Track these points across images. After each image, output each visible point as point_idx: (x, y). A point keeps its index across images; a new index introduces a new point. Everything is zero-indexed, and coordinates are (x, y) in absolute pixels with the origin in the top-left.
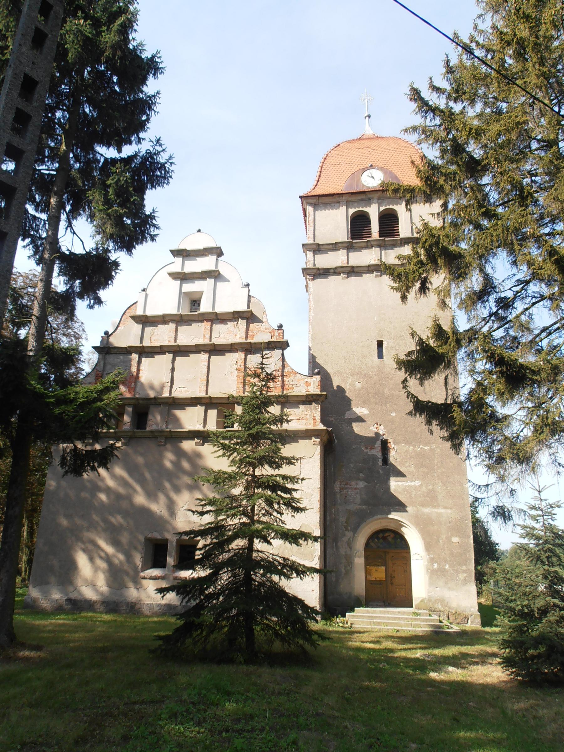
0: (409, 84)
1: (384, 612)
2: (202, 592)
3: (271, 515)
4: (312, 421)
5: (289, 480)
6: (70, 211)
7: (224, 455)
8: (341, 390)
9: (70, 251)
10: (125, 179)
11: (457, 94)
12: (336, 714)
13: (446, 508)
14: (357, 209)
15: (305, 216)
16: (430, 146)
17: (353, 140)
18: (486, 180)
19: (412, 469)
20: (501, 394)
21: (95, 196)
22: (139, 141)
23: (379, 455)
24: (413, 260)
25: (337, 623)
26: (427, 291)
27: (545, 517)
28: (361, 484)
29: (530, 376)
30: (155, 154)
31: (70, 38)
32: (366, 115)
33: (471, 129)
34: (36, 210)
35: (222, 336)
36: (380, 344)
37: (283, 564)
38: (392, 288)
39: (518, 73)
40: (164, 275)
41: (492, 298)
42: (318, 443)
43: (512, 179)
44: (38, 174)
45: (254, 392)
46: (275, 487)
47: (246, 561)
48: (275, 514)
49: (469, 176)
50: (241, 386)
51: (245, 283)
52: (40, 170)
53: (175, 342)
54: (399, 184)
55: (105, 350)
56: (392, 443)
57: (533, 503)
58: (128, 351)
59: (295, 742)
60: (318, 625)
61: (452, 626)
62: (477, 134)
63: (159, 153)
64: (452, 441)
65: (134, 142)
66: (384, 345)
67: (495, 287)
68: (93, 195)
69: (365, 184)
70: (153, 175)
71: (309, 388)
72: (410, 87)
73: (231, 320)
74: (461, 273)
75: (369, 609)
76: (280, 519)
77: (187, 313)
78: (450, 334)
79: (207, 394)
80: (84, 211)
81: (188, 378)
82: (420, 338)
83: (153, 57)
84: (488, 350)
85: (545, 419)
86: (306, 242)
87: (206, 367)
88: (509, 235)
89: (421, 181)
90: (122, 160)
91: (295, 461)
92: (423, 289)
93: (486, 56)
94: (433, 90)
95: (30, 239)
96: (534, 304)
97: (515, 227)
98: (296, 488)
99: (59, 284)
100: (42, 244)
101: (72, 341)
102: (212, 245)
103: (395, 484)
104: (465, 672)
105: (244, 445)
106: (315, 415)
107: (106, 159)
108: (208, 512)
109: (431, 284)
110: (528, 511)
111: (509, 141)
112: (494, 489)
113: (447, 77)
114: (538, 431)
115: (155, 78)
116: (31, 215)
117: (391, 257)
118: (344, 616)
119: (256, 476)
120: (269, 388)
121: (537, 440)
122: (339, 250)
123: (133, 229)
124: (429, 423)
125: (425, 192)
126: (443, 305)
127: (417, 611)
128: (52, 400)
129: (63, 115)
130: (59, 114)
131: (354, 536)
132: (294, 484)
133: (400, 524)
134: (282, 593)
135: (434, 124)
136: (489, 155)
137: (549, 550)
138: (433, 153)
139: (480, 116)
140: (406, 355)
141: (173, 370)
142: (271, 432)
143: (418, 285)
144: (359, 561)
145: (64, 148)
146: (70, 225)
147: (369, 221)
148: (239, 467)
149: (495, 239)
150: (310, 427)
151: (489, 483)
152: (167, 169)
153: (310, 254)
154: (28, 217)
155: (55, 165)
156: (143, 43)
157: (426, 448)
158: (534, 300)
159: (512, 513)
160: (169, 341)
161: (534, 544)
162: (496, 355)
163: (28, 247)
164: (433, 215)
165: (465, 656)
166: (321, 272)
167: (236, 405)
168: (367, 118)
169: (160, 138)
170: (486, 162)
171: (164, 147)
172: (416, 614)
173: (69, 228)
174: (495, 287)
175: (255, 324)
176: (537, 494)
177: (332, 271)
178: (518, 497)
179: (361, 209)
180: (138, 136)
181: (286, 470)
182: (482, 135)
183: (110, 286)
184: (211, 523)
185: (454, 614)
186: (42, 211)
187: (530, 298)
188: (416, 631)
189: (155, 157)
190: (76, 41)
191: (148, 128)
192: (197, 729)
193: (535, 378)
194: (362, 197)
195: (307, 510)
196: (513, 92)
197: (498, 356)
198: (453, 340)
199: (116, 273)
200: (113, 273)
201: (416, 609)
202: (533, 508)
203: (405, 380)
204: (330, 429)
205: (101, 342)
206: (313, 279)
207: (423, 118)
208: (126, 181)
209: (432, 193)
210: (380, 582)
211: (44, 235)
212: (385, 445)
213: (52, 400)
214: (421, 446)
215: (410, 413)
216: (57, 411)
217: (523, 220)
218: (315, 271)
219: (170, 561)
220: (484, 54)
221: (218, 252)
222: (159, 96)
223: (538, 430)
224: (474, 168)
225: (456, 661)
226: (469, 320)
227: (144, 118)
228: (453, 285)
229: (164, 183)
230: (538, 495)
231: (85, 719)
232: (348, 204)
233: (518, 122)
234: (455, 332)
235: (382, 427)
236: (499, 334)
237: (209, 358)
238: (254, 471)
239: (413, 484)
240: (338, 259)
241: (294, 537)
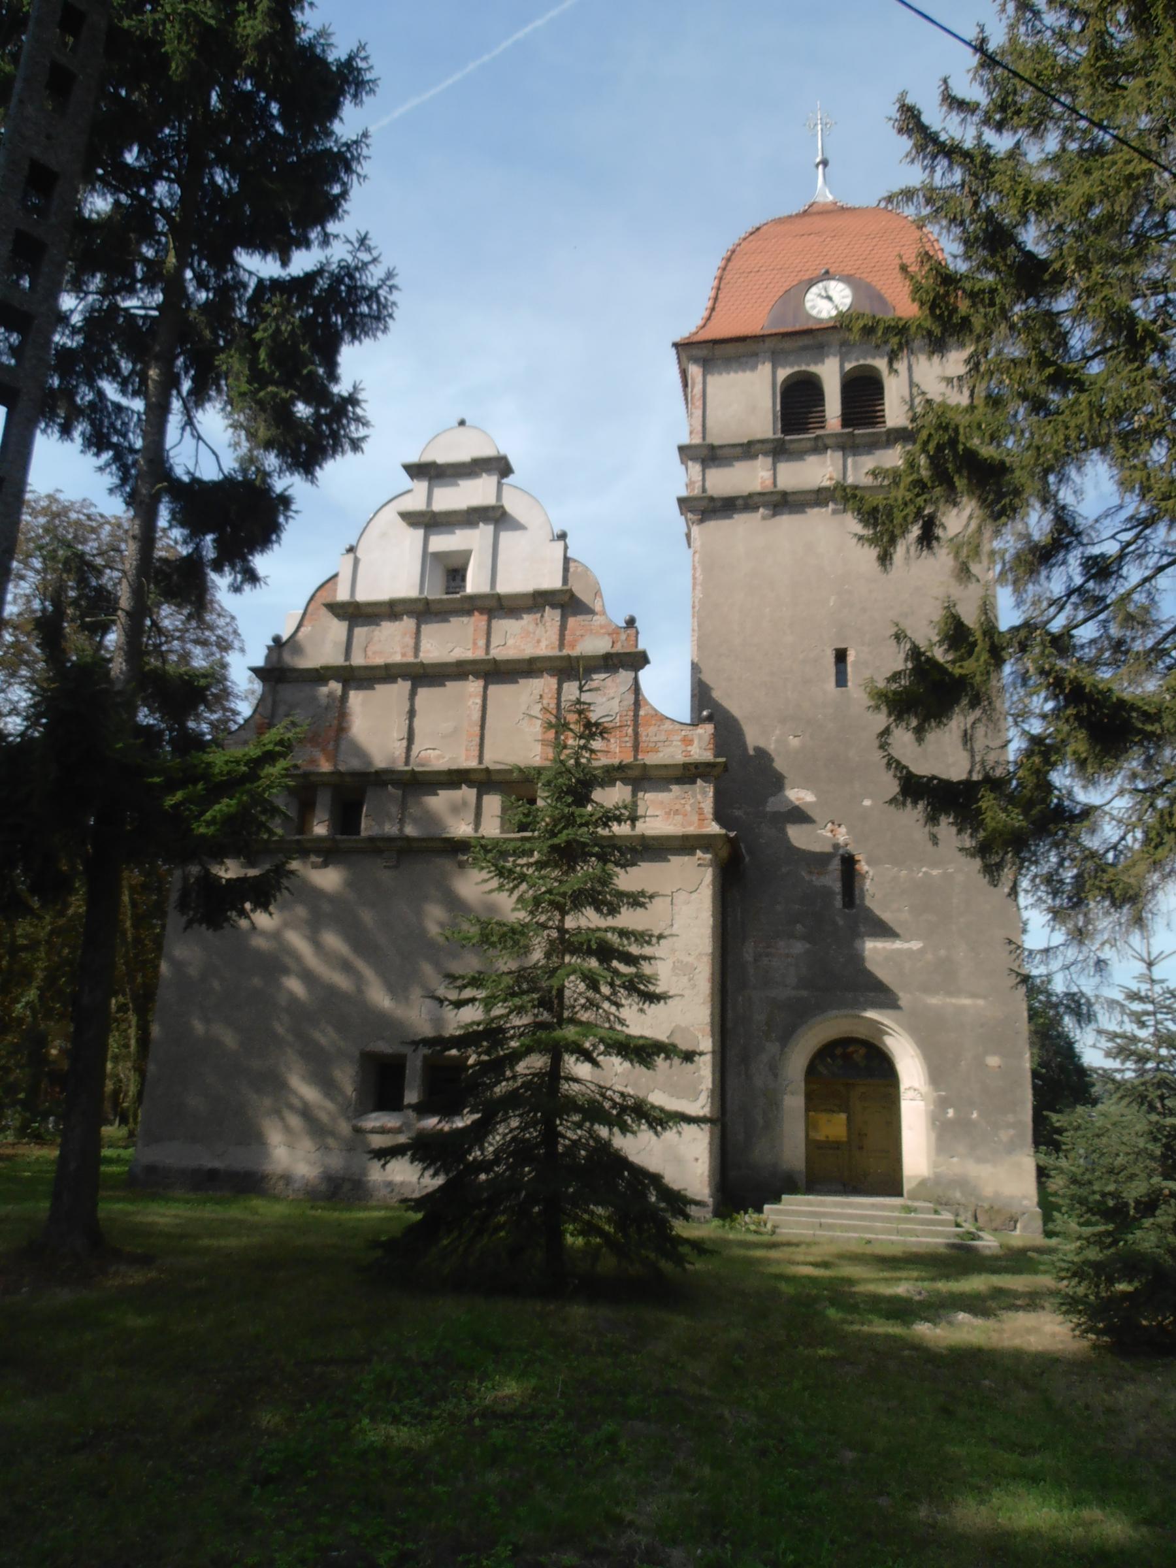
0: (895, 97)
1: (842, 1205)
2: (462, 1157)
3: (598, 1007)
4: (695, 818)
5: (633, 939)
6: (190, 393)
7: (501, 888)
9: (192, 474)
10: (289, 328)
11: (1003, 113)
12: (706, 1392)
13: (974, 996)
14: (796, 369)
15: (685, 385)
16: (944, 231)
17: (790, 217)
18: (1064, 303)
19: (905, 915)
20: (1082, 764)
21: (232, 362)
22: (326, 240)
23: (837, 887)
24: (903, 478)
25: (746, 1223)
26: (935, 543)
27: (1159, 1016)
28: (799, 947)
29: (1140, 726)
30: (357, 268)
31: (171, 30)
32: (818, 160)
33: (1027, 192)
34: (124, 392)
35: (510, 642)
36: (841, 656)
37: (621, 1105)
38: (861, 538)
39: (1136, 61)
40: (390, 515)
41: (1074, 560)
43: (1110, 303)
44: (124, 317)
45: (562, 762)
46: (605, 953)
47: (548, 1097)
48: (606, 1005)
49: (1024, 294)
51: (557, 531)
52: (126, 310)
53: (416, 655)
54: (874, 317)
55: (277, 672)
56: (863, 863)
57: (1134, 986)
58: (321, 675)
59: (612, 1440)
60: (701, 1227)
61: (980, 1233)
62: (1043, 200)
63: (365, 265)
64: (983, 858)
65: (316, 243)
66: (851, 657)
67: (1079, 534)
68: (228, 363)
69: (814, 313)
70: (355, 313)
71: (689, 748)
72: (898, 105)
73: (529, 609)
74: (1004, 507)
75: (811, 1197)
76: (615, 1016)
77: (438, 597)
78: (978, 635)
80: (219, 390)
81: (447, 732)
82: (913, 643)
83: (351, 59)
84: (1051, 669)
85: (1166, 817)
86: (686, 440)
87: (478, 707)
88: (1104, 424)
89: (920, 308)
90: (295, 280)
91: (647, 900)
92: (928, 538)
93: (1070, 26)
94: (950, 107)
95: (111, 453)
96: (1161, 569)
97: (1117, 407)
98: (648, 954)
99: (173, 540)
100: (135, 463)
101: (213, 654)
102: (487, 452)
103: (873, 948)
104: (990, 1323)
105: (542, 868)
106: (702, 805)
107: (261, 281)
108: (472, 1000)
109: (945, 528)
110: (1126, 1003)
111: (1110, 218)
112: (1061, 958)
113: (982, 77)
114: (1153, 841)
115: (356, 104)
116: (113, 403)
117: (860, 470)
118: (759, 1210)
119: (567, 931)
120: (592, 751)
121: (1150, 860)
123: (313, 428)
124: (932, 819)
125: (930, 333)
126: (964, 573)
127: (909, 1203)
128: (157, 780)
129: (169, 191)
130: (161, 188)
131: (782, 1050)
132: (642, 947)
133: (879, 1030)
134: (620, 1162)
135: (949, 184)
136: (1065, 251)
137: (1165, 1082)
138: (949, 248)
139: (1054, 161)
140: (888, 680)
141: (412, 713)
142: (597, 840)
143: (916, 531)
144: (794, 1102)
145: (174, 260)
146: (190, 422)
148: (531, 912)
149: (1073, 435)
150: (692, 830)
151: (1053, 944)
152: (382, 299)
153: (695, 468)
154: (106, 407)
155: (156, 296)
156: (330, 31)
157: (935, 872)
158: (1165, 560)
159: (1097, 1007)
160: (404, 655)
161: (1134, 1071)
162: (1067, 682)
163: (108, 470)
164: (949, 381)
165: (998, 1293)
166: (719, 504)
168: (821, 167)
169: (367, 234)
170: (1057, 266)
171: (375, 253)
172: (908, 1209)
173: (188, 429)
174: (1079, 534)
175: (580, 618)
176: (1141, 967)
177: (740, 502)
178: (1110, 975)
179: (804, 368)
180: (323, 228)
181: (628, 918)
182: (1053, 204)
183: (276, 546)
184: (478, 1024)
185: (986, 1211)
186: (135, 394)
187: (1157, 556)
188: (905, 1243)
189: (357, 275)
190: (185, 37)
191: (345, 211)
192: (427, 1410)
193: (1149, 728)
195: (670, 997)
196: (1121, 107)
197: (1071, 682)
198: (982, 649)
199: (287, 518)
200: (281, 519)
201: (909, 1198)
202: (1134, 996)
203: (886, 732)
204: (732, 834)
205: (268, 658)
206: (701, 521)
207: (928, 171)
208: (293, 331)
209: (947, 334)
210: (835, 1146)
211: (139, 444)
212: (849, 862)
213: (157, 780)
214: (924, 869)
215: (893, 801)
216: (170, 801)
217: (1133, 392)
218: (705, 503)
220: (1064, 21)
221: (500, 467)
222: (368, 142)
223: (1152, 839)
224: (1033, 277)
225: (977, 1305)
226: (1019, 604)
227: (336, 189)
228: (987, 533)
229: (377, 329)
230: (1146, 971)
231: (219, 1387)
232: (777, 359)
233: (1131, 174)
234: (990, 630)
235: (843, 830)
236: (1086, 633)
238: (562, 921)
239: (906, 946)
240: (753, 476)
241: (642, 1052)
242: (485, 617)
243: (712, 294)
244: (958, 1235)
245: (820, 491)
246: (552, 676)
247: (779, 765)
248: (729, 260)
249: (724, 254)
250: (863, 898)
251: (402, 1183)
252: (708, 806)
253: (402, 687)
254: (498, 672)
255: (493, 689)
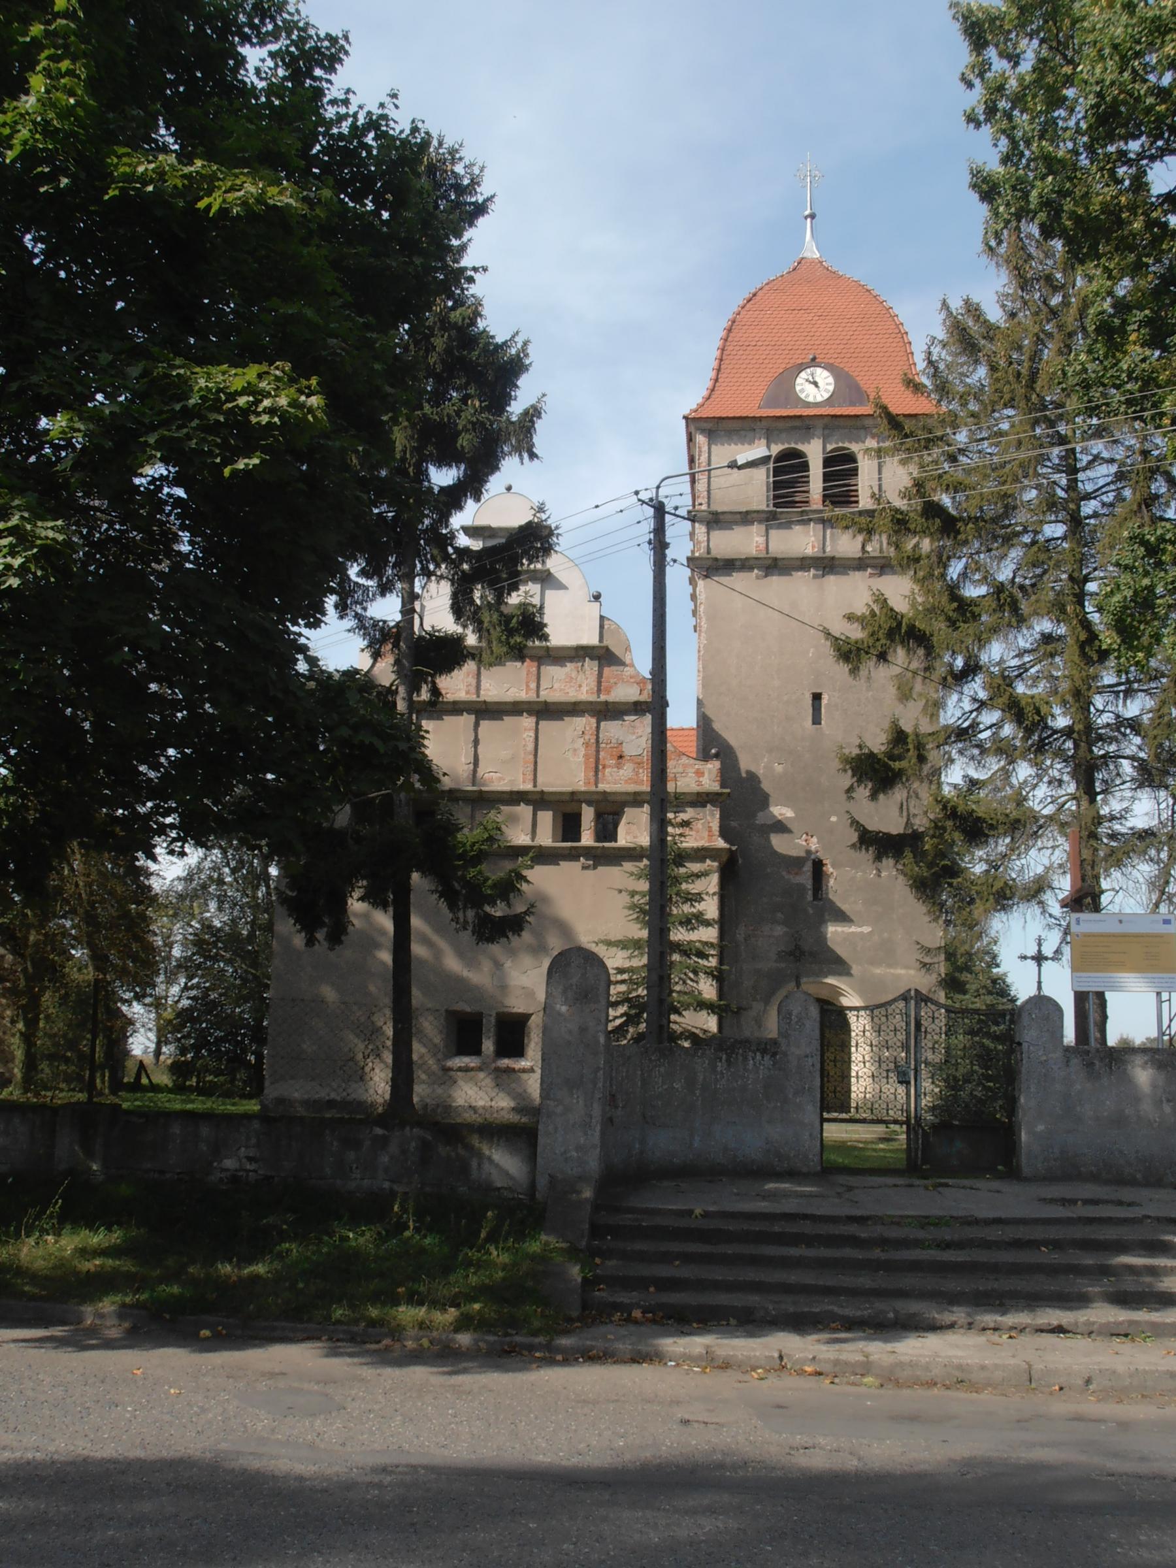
8: (753, 778)
14: (786, 446)
23: (809, 884)
28: (779, 930)
32: (808, 212)
35: (556, 686)
36: (817, 697)
42: (715, 869)
50: (592, 774)
51: (593, 591)
66: (825, 700)
73: (571, 659)
79: (535, 786)
87: (532, 739)
103: (834, 931)
122: (752, 523)
133: (837, 992)
141: (476, 742)
147: (804, 467)
153: (701, 529)
160: (467, 693)
167: (584, 805)
175: (614, 668)
177: (738, 563)
179: (793, 445)
194: (797, 423)
212: (818, 865)
215: (853, 846)
218: (709, 563)
219: (488, 1046)
235: (815, 840)
237: (537, 724)
239: (859, 930)
240: (747, 541)
242: (536, 664)
243: (715, 364)
244: (886, 1133)
245: (803, 559)
246: (592, 716)
247: (766, 786)
248: (729, 330)
249: (725, 323)
250: (827, 894)
251: (484, 1107)
252: (715, 825)
253: (468, 719)
254: (546, 711)
255: (542, 723)
